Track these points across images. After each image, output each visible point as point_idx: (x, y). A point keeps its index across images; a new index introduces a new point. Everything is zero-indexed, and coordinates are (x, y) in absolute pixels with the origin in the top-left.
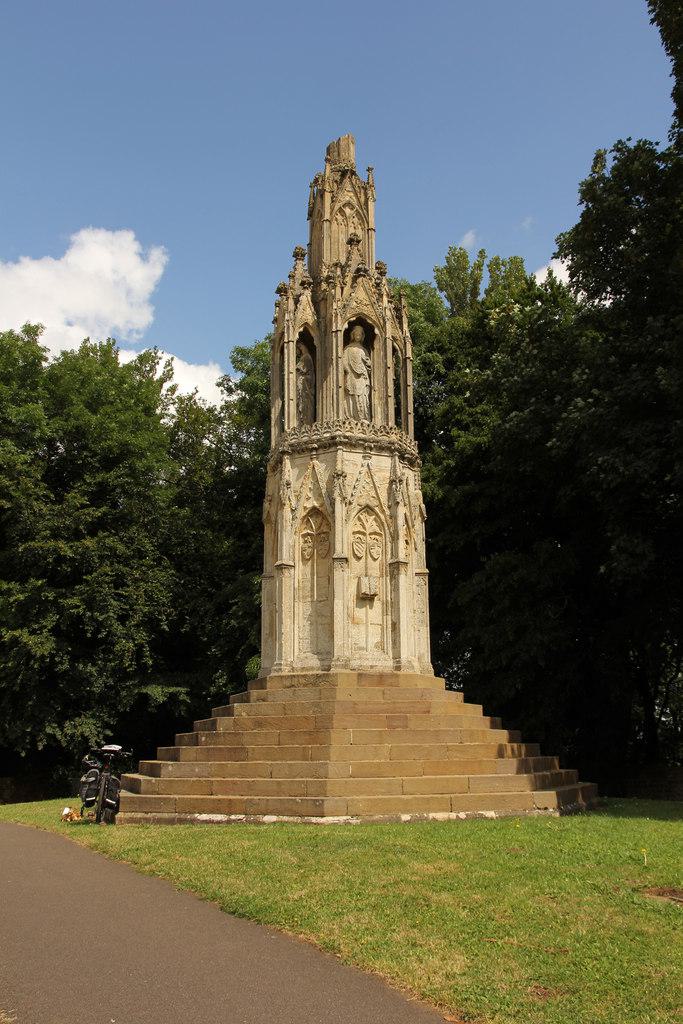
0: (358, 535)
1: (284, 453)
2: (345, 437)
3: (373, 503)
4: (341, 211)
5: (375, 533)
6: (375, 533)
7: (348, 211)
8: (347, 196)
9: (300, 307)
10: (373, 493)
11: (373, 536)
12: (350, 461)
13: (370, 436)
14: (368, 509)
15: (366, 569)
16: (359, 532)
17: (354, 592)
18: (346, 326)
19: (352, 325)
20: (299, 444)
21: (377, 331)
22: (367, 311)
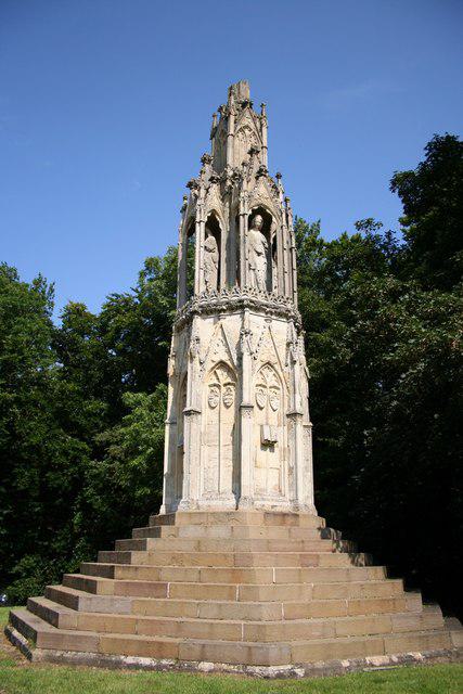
0: (260, 388)
1: (195, 312)
2: (252, 301)
3: (274, 360)
4: (241, 130)
5: (275, 387)
6: (275, 387)
7: (247, 131)
8: (247, 121)
9: (209, 197)
10: (273, 352)
11: (273, 390)
12: (255, 321)
13: (271, 303)
14: (222, 364)
15: (267, 418)
16: (215, 385)
17: (243, 435)
18: (250, 212)
19: (255, 212)
20: (208, 305)
21: (274, 219)
22: (268, 203)
